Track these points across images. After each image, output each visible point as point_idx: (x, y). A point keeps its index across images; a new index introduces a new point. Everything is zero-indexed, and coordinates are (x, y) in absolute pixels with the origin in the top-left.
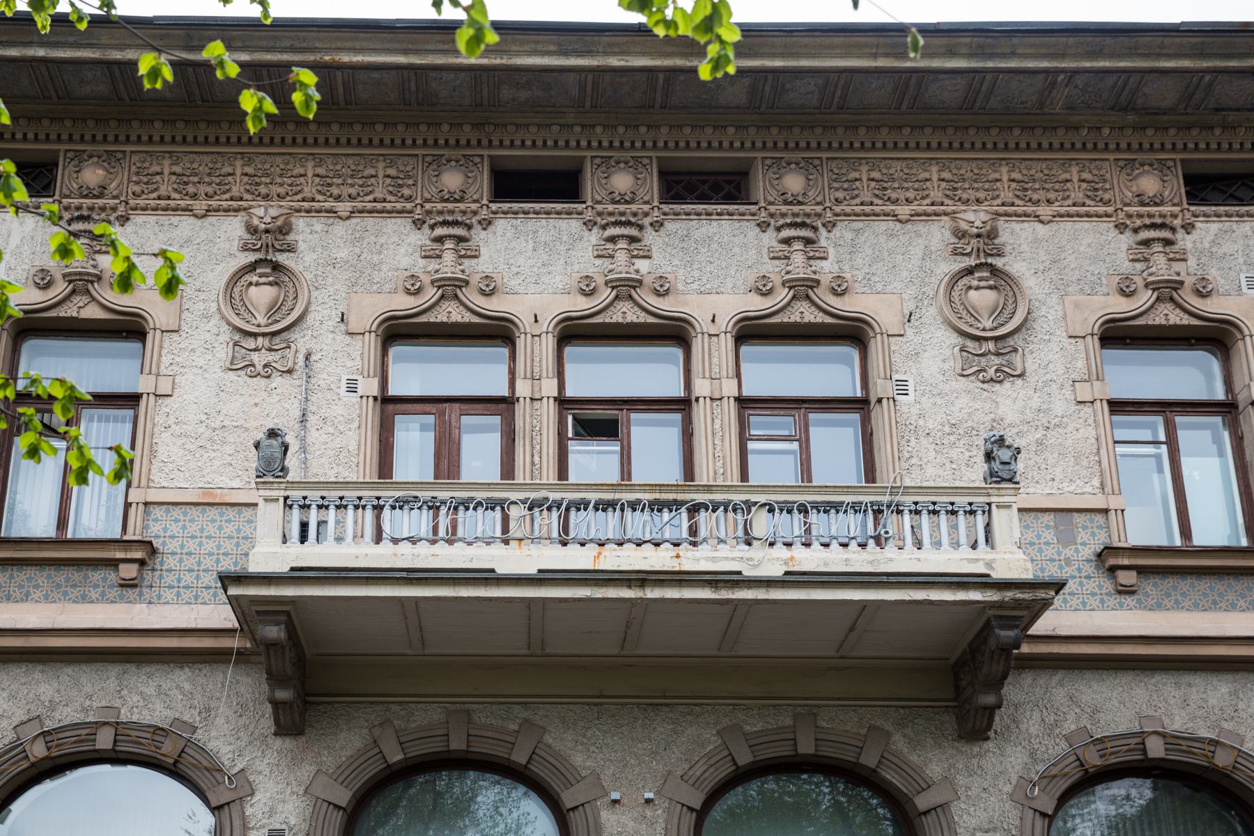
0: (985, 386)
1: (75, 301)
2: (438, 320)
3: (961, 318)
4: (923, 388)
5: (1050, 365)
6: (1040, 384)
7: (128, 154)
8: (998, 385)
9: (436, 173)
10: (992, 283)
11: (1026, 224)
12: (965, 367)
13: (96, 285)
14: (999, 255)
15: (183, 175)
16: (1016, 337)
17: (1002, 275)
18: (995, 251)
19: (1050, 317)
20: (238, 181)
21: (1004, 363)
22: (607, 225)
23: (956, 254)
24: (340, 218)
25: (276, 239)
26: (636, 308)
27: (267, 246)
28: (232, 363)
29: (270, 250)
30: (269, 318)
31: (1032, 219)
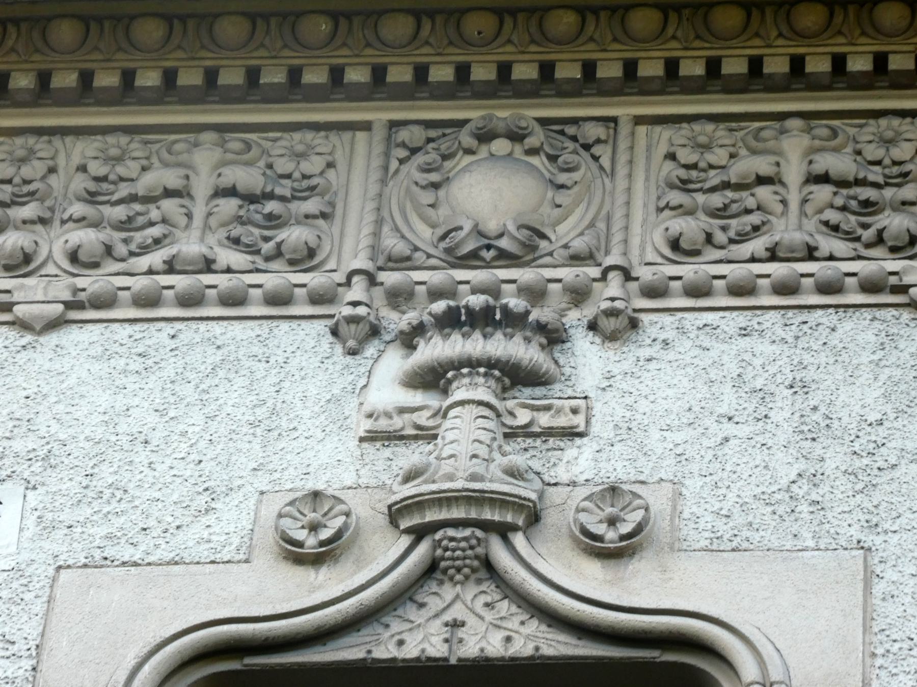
1: (435, 604)
2: (411, 651)
7: (624, 129)
9: (434, 177)
13: (519, 540)
20: (794, 205)
22: (419, 330)
24: (24, 325)
26: (504, 606)
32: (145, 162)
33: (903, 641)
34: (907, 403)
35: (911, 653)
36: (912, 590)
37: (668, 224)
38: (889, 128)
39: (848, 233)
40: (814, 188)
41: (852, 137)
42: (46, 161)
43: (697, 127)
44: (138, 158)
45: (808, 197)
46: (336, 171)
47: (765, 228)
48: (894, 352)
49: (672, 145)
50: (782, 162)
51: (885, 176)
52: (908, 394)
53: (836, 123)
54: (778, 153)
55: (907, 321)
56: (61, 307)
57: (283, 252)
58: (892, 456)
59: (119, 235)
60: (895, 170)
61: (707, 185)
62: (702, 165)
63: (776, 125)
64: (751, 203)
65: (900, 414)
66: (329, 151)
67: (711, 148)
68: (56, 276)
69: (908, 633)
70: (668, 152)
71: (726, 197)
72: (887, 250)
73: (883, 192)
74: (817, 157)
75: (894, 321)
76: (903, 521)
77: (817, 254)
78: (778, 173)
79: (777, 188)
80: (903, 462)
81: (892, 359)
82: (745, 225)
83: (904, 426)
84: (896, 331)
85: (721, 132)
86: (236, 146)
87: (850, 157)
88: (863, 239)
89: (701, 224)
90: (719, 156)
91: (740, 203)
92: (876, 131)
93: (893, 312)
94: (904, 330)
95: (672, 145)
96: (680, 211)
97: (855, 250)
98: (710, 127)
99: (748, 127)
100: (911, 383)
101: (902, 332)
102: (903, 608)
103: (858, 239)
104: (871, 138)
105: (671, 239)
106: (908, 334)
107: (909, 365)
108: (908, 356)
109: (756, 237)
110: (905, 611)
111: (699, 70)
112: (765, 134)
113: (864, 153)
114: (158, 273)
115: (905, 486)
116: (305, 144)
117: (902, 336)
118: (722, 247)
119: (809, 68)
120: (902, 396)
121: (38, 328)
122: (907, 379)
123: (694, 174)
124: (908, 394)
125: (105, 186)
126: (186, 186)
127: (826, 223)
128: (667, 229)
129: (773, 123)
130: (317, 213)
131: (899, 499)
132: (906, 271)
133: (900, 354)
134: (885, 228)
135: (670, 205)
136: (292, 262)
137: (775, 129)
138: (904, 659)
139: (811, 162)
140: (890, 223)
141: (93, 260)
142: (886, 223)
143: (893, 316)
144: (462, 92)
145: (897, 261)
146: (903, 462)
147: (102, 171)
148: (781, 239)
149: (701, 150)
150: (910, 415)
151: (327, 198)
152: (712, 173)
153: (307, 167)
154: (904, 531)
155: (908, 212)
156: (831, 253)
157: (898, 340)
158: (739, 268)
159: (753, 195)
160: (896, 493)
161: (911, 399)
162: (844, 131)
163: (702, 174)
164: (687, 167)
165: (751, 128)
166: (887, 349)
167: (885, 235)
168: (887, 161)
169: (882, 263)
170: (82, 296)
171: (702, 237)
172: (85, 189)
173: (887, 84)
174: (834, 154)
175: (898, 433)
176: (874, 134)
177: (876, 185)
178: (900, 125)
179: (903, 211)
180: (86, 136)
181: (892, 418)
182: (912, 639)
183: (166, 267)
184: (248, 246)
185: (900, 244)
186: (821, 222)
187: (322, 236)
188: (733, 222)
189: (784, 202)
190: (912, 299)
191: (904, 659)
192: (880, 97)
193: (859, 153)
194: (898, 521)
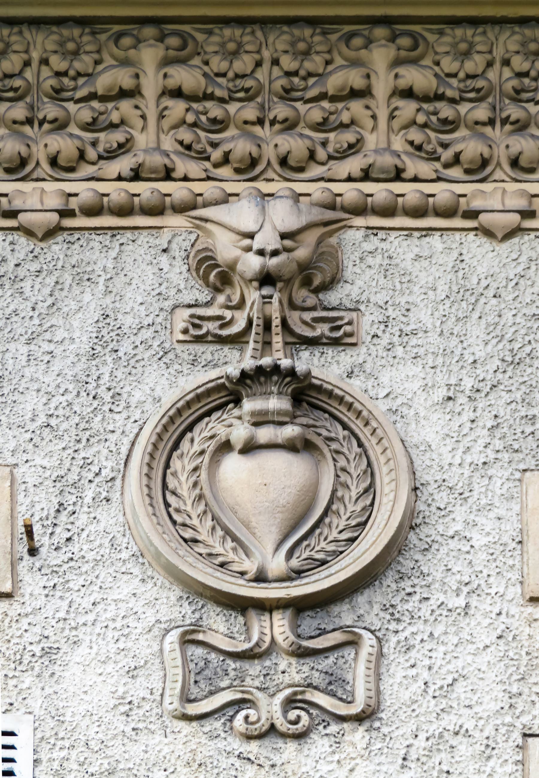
0: (254, 747)
4: (57, 754)
5: (460, 687)
6: (421, 743)
8: (291, 746)
11: (435, 240)
12: (194, 691)
14: (336, 342)
15: (208, 97)
16: (361, 599)
18: (323, 329)
19: (479, 540)
21: (317, 678)
23: (199, 339)
25: (293, 306)
27: (267, 326)
29: (277, 340)
30: (290, 554)
31: (457, 222)
32: (327, 56)
59: (88, 136)
64: (115, 117)
68: (503, 181)
77: (404, 175)
88: (443, 159)
97: (206, 170)
99: (110, 29)
125: (296, 80)
136: (238, 171)
147: (62, 66)
158: (215, 187)
162: (425, 39)
172: (282, 86)
183: (132, 174)
184: (427, 153)
189: (143, 117)
190: (480, 224)
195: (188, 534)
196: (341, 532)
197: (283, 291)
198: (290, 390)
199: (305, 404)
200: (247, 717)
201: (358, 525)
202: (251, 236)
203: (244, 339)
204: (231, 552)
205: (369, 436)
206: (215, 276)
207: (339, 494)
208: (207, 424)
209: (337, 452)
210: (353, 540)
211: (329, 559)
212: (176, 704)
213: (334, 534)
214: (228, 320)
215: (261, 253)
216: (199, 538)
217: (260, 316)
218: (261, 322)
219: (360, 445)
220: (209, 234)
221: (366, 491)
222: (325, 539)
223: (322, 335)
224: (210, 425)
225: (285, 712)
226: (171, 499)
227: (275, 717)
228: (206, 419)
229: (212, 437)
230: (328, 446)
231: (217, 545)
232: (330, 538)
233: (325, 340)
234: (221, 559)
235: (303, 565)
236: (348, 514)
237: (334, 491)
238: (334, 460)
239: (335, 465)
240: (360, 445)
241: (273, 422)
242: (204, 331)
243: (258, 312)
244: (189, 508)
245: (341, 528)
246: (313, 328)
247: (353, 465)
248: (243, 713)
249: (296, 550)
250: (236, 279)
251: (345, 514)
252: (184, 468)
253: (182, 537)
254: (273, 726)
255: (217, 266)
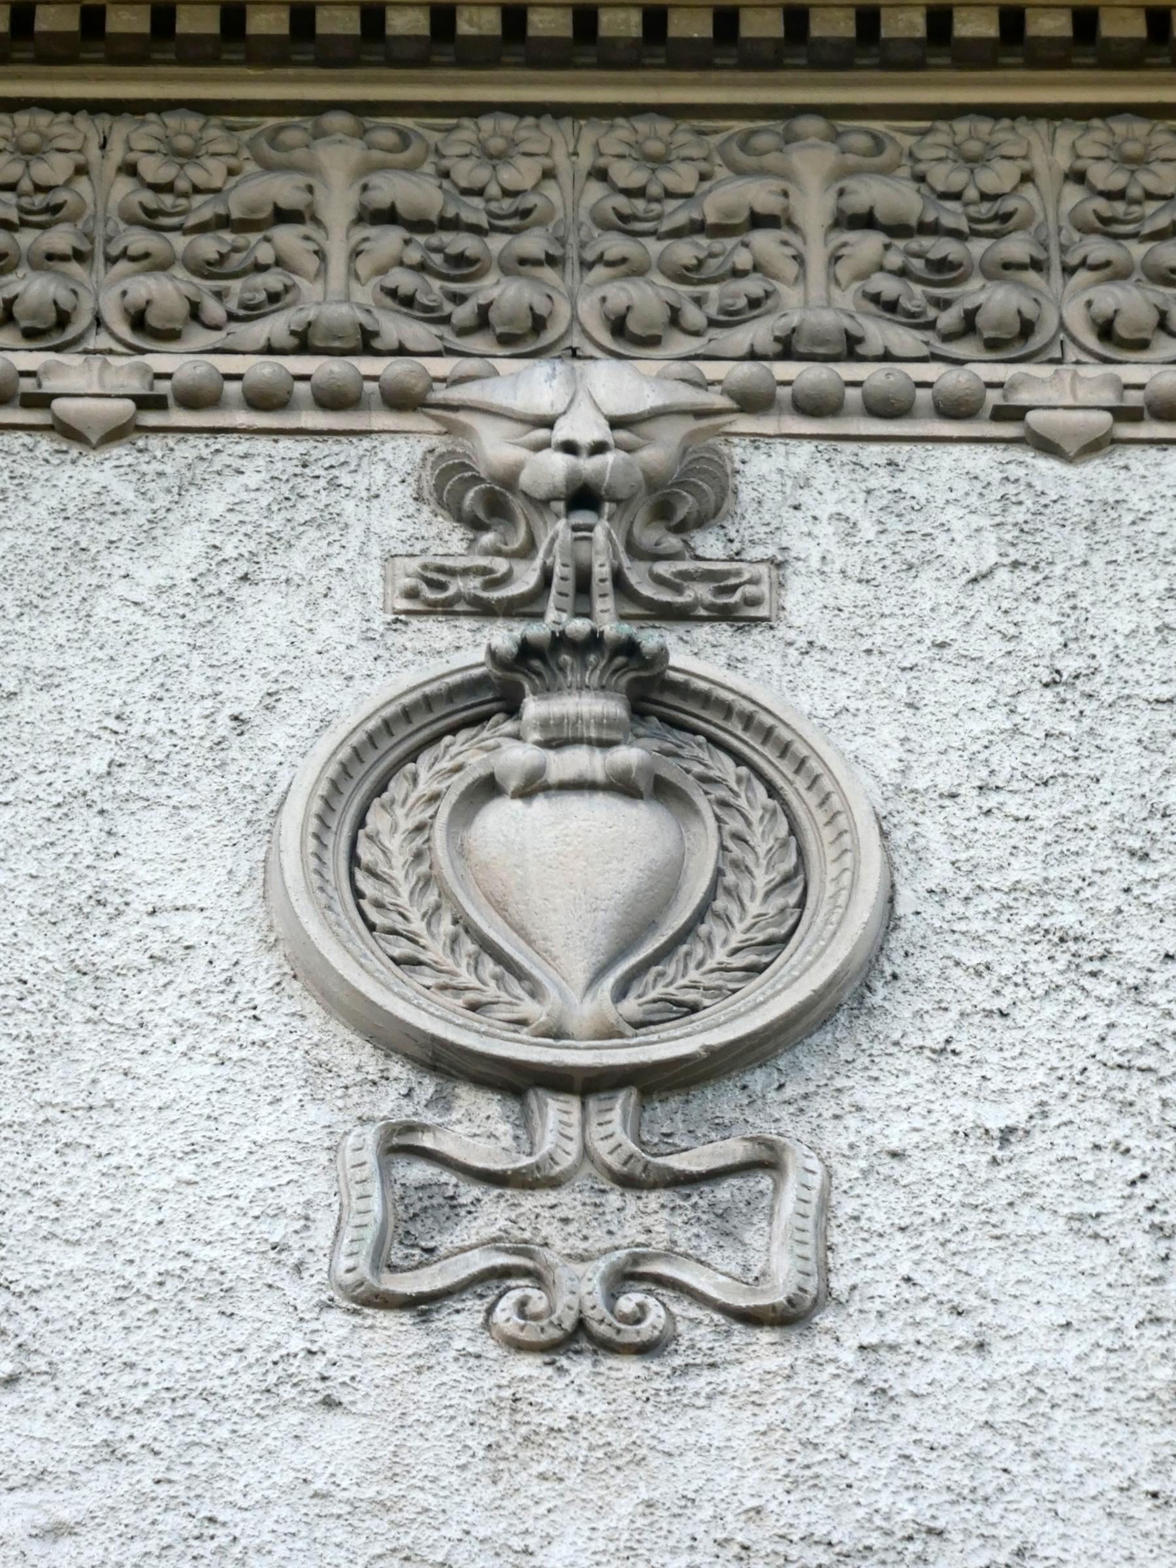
3: (411, 962)
10: (629, 756)
12: (397, 1254)
14: (724, 614)
17: (711, 723)
24: (68, 432)
28: (381, 1262)
30: (621, 992)
33: (9, 983)
34: (40, 591)
35: (23, 1004)
36: (29, 900)
37: (126, 284)
38: (31, 129)
39: (912, 315)
40: (851, 236)
41: (906, 151)
42: (223, 159)
43: (173, 121)
44: (692, 159)
45: (840, 253)
46: (1036, 187)
47: (289, 298)
48: (23, 505)
49: (131, 150)
50: (792, 190)
51: (22, 209)
52: (42, 576)
53: (408, 123)
54: (784, 175)
55: (46, 455)
56: (130, 404)
57: (16, 315)
58: (9, 678)
60: (39, 200)
61: (192, 221)
62: (655, 190)
63: (779, 126)
65: (26, 610)
66: (78, 147)
67: (669, 162)
69: (18, 971)
70: (1071, 168)
71: (698, 246)
72: (981, 345)
73: (17, 236)
74: (375, 180)
75: (25, 454)
76: (21, 786)
77: (377, 344)
78: (310, 205)
79: (307, 229)
80: (27, 688)
81: (19, 517)
82: (736, 296)
83: (32, 629)
84: (27, 471)
85: (683, 135)
86: (387, 138)
87: (432, 180)
89: (182, 287)
90: (211, 172)
91: (721, 259)
92: (9, 133)
93: (24, 438)
94: (40, 469)
95: (131, 150)
96: (623, 268)
98: (664, 126)
100: (48, 558)
101: (37, 473)
102: (14, 929)
103: (445, 320)
104: (465, 149)
105: (1100, 321)
106: (47, 475)
107: (45, 529)
108: (45, 513)
109: (274, 311)
110: (16, 935)
111: (1136, 28)
112: (289, 137)
113: (930, 179)
114: (765, 358)
115: (27, 728)
116: (502, 136)
117: (36, 480)
118: (697, 334)
119: (464, 27)
120: (32, 579)
121: (94, 439)
122: (41, 551)
123: (168, 200)
124: (42, 576)
126: (310, 205)
127: (392, 293)
128: (124, 293)
129: (772, 123)
130: (69, 252)
131: (16, 751)
132: (48, 370)
133: (31, 509)
134: (16, 297)
135: (1090, 261)
137: (778, 134)
138: (9, 1014)
139: (365, 188)
140: (25, 291)
141: (169, 326)
142: (17, 288)
143: (24, 445)
144: (1154, 56)
145: (36, 354)
146: (27, 688)
148: (318, 317)
149: (650, 165)
150: (43, 612)
151: (80, 225)
152: (198, 200)
153: (512, 176)
154: (21, 804)
155: (57, 272)
156: (400, 343)
157: (29, 486)
159: (267, 240)
160: (12, 740)
161: (46, 584)
162: (421, 137)
163: (183, 202)
164: (157, 188)
165: (731, 132)
166: (11, 500)
167: (493, 315)
168: (26, 185)
169: (9, 356)
170: (163, 387)
171: (183, 309)
173: (876, 60)
174: (407, 175)
175: (21, 642)
176: (6, 138)
177: (476, 230)
178: (50, 125)
179: (48, 270)
180: (595, 120)
181: (12, 616)
182: (25, 982)
185: (41, 326)
186: (383, 289)
187: (554, 296)
188: (236, 285)
189: (799, 259)
190: (55, 417)
191: (9, 1014)
192: (19, 77)
193: (445, 174)
194: (13, 787)
195: (402, 948)
196: (735, 952)
197: (616, 519)
198: (624, 681)
199: (654, 719)
200: (522, 1304)
201: (768, 942)
202: (548, 423)
203: (535, 609)
204: (492, 983)
205: (791, 776)
206: (473, 499)
207: (730, 878)
208: (447, 747)
209: (723, 804)
210: (755, 970)
211: (707, 1002)
212: (365, 1270)
213: (720, 955)
214: (499, 575)
215: (570, 448)
216: (423, 957)
217: (568, 561)
218: (569, 572)
219: (773, 791)
220: (464, 431)
221: (787, 879)
222: (700, 964)
223: (697, 603)
224: (453, 750)
225: (612, 1296)
226: (366, 884)
227: (589, 1302)
228: (448, 739)
229: (458, 769)
230: (707, 793)
231: (463, 971)
232: (711, 964)
233: (702, 612)
234: (471, 996)
235: (652, 1012)
236: (749, 921)
237: (719, 873)
238: (718, 819)
239: (720, 828)
240: (773, 791)
241: (590, 742)
242: (451, 591)
243: (562, 554)
244: (404, 900)
245: (734, 944)
246: (678, 590)
247: (758, 829)
248: (514, 1296)
249: (635, 983)
250: (517, 505)
251: (741, 920)
252: (394, 828)
253: (393, 959)
254: (581, 1324)
255: (477, 479)
